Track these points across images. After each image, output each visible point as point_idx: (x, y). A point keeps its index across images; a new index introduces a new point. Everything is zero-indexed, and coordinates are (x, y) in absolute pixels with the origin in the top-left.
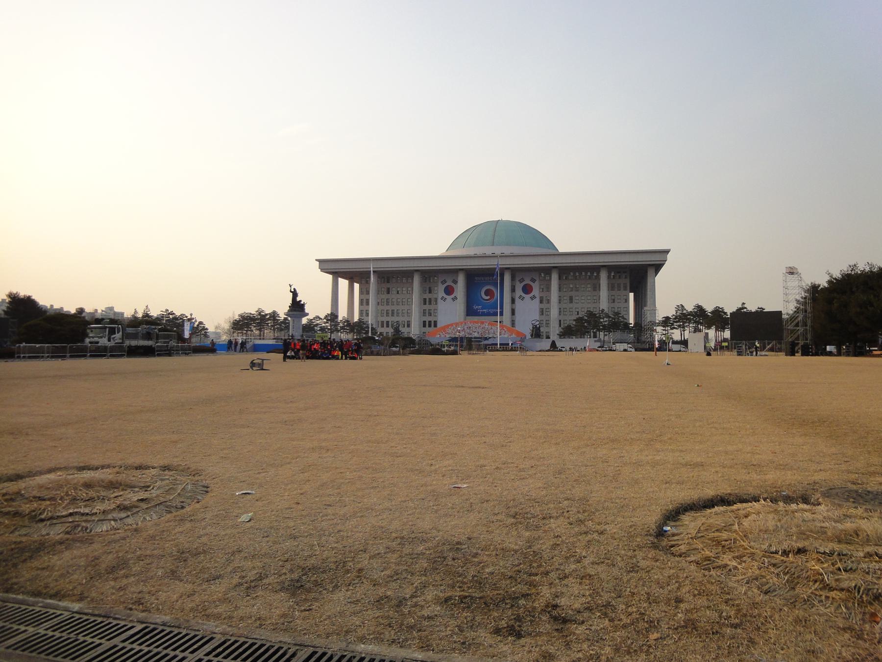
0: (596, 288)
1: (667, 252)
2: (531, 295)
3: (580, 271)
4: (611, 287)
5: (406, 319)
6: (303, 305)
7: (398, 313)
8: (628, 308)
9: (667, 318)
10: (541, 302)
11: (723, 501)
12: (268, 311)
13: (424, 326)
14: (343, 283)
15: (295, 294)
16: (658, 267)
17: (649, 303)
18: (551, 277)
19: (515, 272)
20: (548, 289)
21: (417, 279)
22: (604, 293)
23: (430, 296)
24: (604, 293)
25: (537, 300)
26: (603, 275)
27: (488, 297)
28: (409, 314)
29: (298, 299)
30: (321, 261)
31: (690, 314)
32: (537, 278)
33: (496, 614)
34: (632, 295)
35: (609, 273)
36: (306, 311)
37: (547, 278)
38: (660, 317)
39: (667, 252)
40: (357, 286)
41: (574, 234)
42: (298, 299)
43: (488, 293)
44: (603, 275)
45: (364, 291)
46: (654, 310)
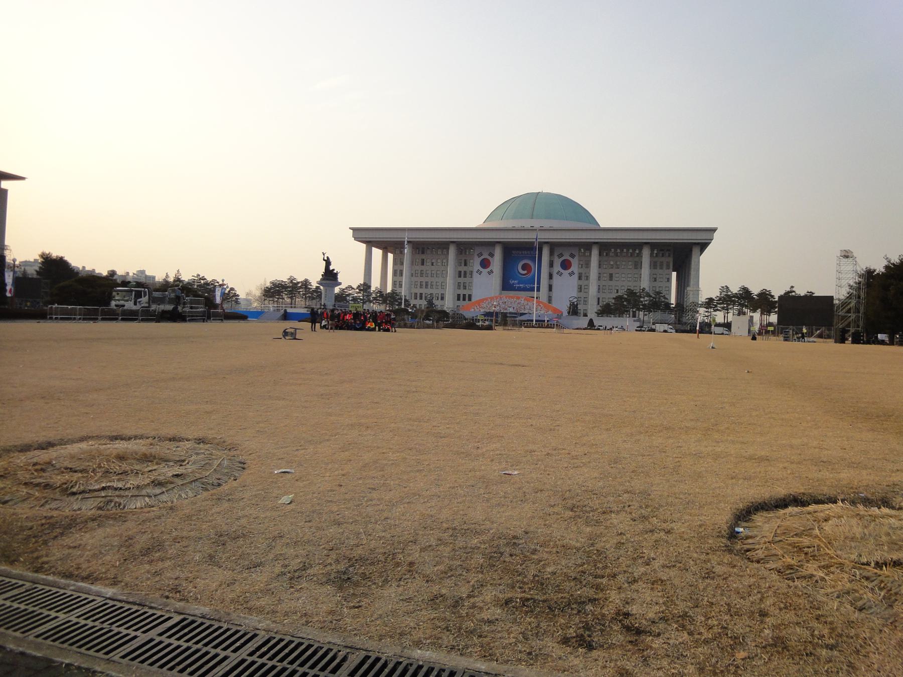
0: (638, 265)
1: (714, 230)
2: (570, 271)
3: (621, 248)
5: (440, 291)
6: (336, 274)
7: (427, 285)
9: (711, 300)
10: (580, 278)
12: (300, 279)
13: (459, 299)
14: (377, 253)
15: (328, 262)
16: (703, 246)
18: (448, 253)
19: (554, 246)
20: (588, 265)
21: (452, 251)
22: (646, 271)
24: (646, 271)
25: (576, 276)
26: (646, 252)
27: (525, 272)
28: (443, 286)
29: (331, 268)
30: (355, 230)
31: (735, 295)
34: (674, 274)
35: (652, 251)
36: (339, 280)
38: (703, 298)
39: (714, 230)
40: (390, 256)
41: (618, 208)
42: (331, 268)
44: (646, 252)
45: (398, 262)
46: (698, 290)
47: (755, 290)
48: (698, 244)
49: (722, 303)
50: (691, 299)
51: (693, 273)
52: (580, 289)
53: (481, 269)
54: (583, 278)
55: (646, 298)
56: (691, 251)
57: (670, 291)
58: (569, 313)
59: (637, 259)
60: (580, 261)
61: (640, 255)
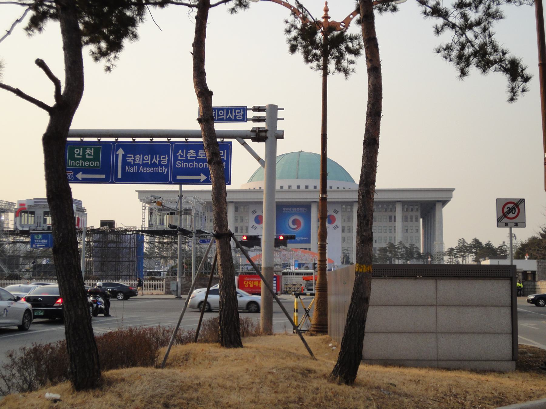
0: (392, 219)
1: (452, 190)
2: (334, 225)
4: (405, 219)
8: (419, 237)
9: (452, 249)
10: (343, 231)
11: (488, 360)
16: (444, 203)
17: (437, 239)
20: (350, 219)
22: (399, 224)
23: (241, 224)
24: (399, 224)
25: (340, 229)
26: (399, 208)
27: (295, 227)
31: (471, 247)
32: (339, 210)
33: (300, 254)
34: (421, 220)
35: (403, 206)
37: (349, 210)
38: (446, 249)
39: (452, 190)
43: (295, 222)
44: (399, 208)
46: (442, 244)
47: (484, 242)
48: (440, 201)
49: (461, 252)
50: (436, 249)
51: (437, 225)
52: (344, 239)
53: (256, 225)
54: (346, 230)
55: (403, 250)
56: (435, 205)
57: (419, 243)
58: (343, 263)
59: (390, 214)
60: (342, 216)
61: (394, 210)
